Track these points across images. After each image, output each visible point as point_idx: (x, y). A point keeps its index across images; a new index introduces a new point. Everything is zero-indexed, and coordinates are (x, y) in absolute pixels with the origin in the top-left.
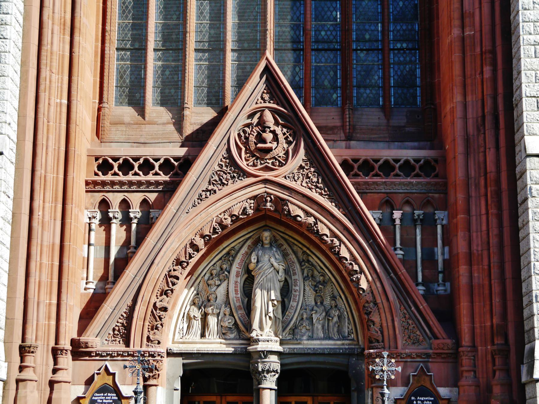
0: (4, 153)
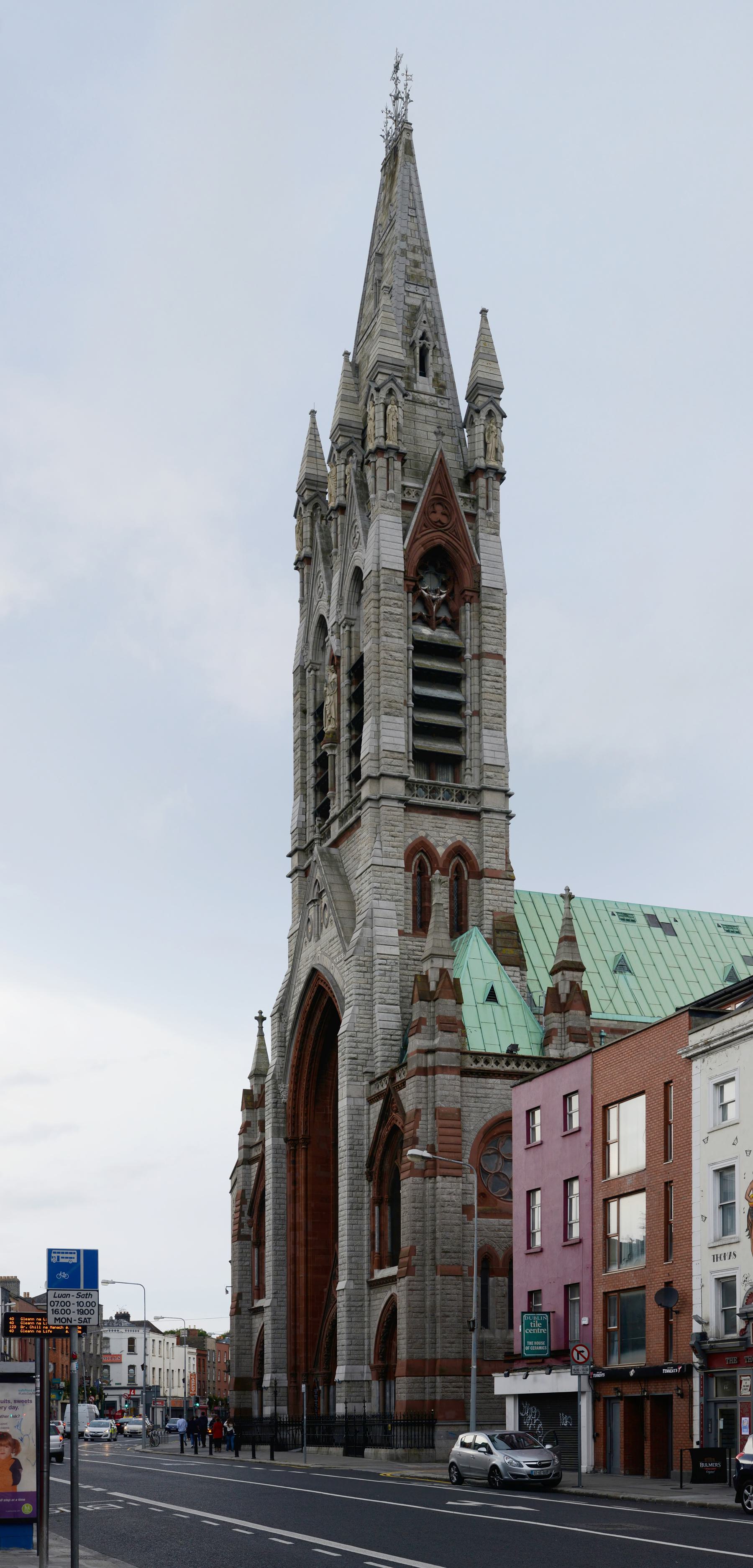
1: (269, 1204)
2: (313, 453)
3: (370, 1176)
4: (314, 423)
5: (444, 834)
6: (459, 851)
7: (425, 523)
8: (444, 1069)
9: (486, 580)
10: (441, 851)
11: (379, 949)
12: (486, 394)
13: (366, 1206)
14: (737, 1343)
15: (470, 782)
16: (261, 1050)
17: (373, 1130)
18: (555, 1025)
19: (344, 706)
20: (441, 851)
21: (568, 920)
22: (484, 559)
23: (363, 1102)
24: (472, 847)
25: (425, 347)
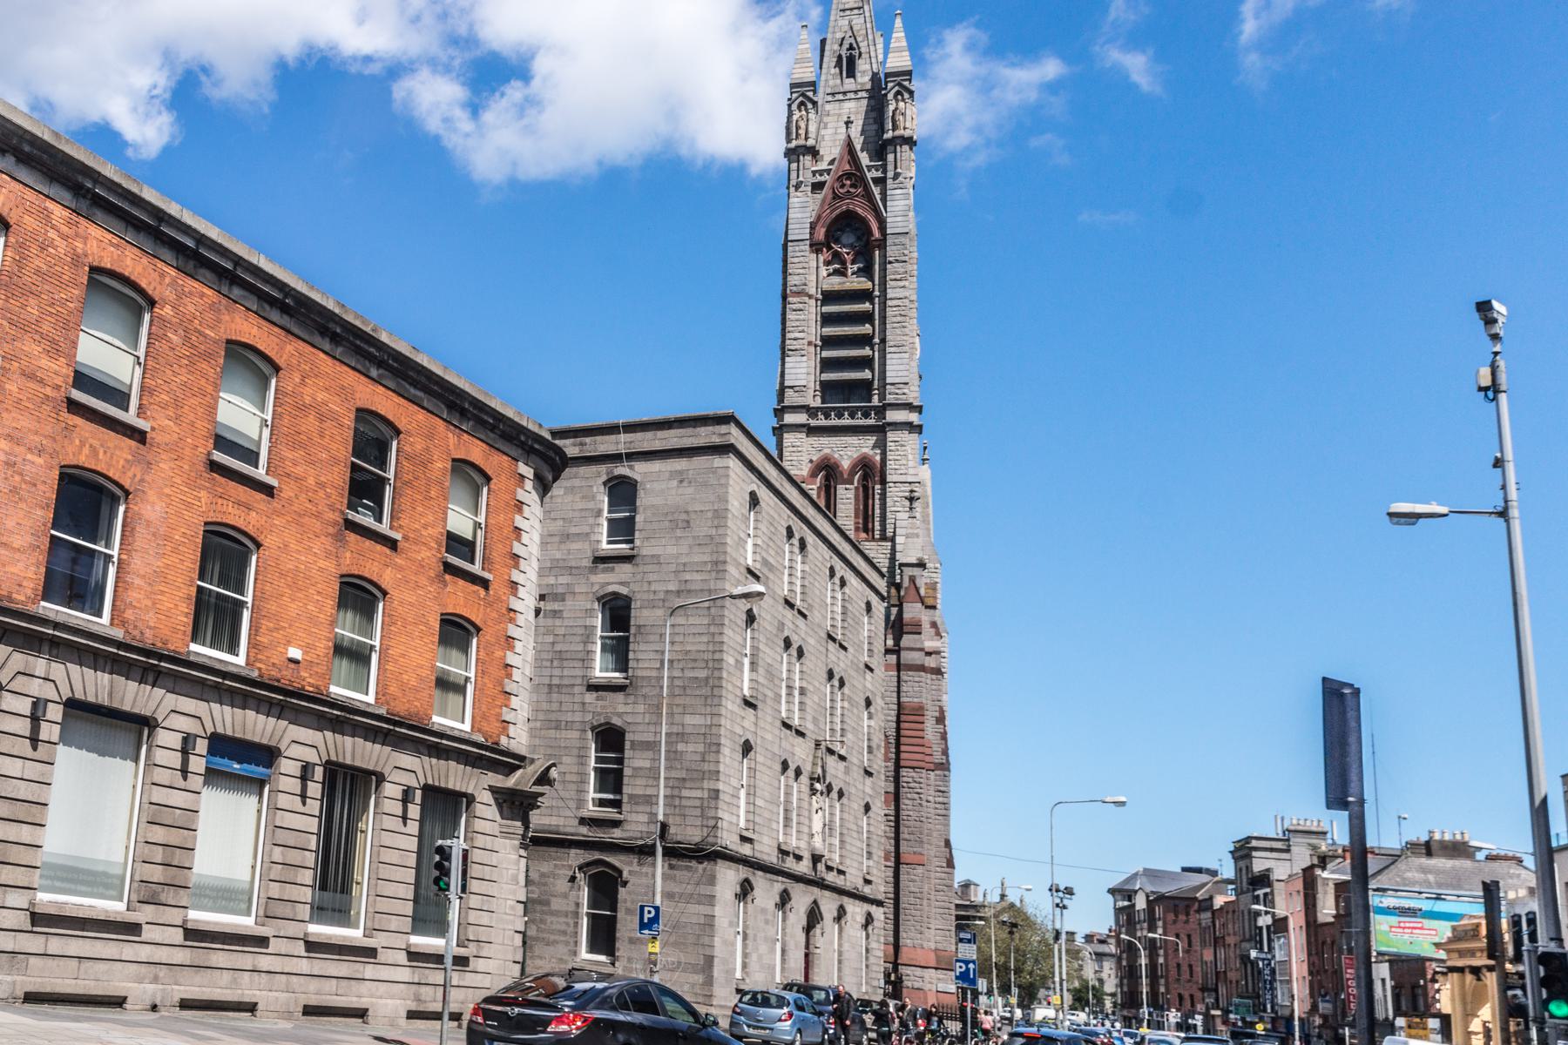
0: (1492, 461)
5: (848, 451)
10: (846, 464)
20: (846, 464)
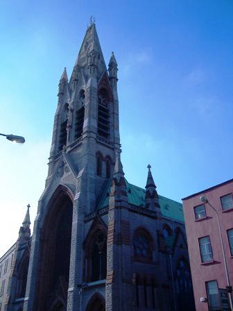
1: (31, 262)
2: (24, 230)
3: (84, 248)
4: (28, 211)
6: (108, 157)
7: (101, 83)
8: (124, 208)
9: (115, 98)
11: (89, 176)
12: (113, 65)
13: (82, 259)
14: (91, 261)
15: (112, 140)
16: (27, 222)
17: (87, 231)
18: (150, 202)
19: (74, 119)
20: (104, 155)
21: (150, 173)
22: (114, 93)
23: (82, 222)
24: (112, 156)
25: (98, 54)
